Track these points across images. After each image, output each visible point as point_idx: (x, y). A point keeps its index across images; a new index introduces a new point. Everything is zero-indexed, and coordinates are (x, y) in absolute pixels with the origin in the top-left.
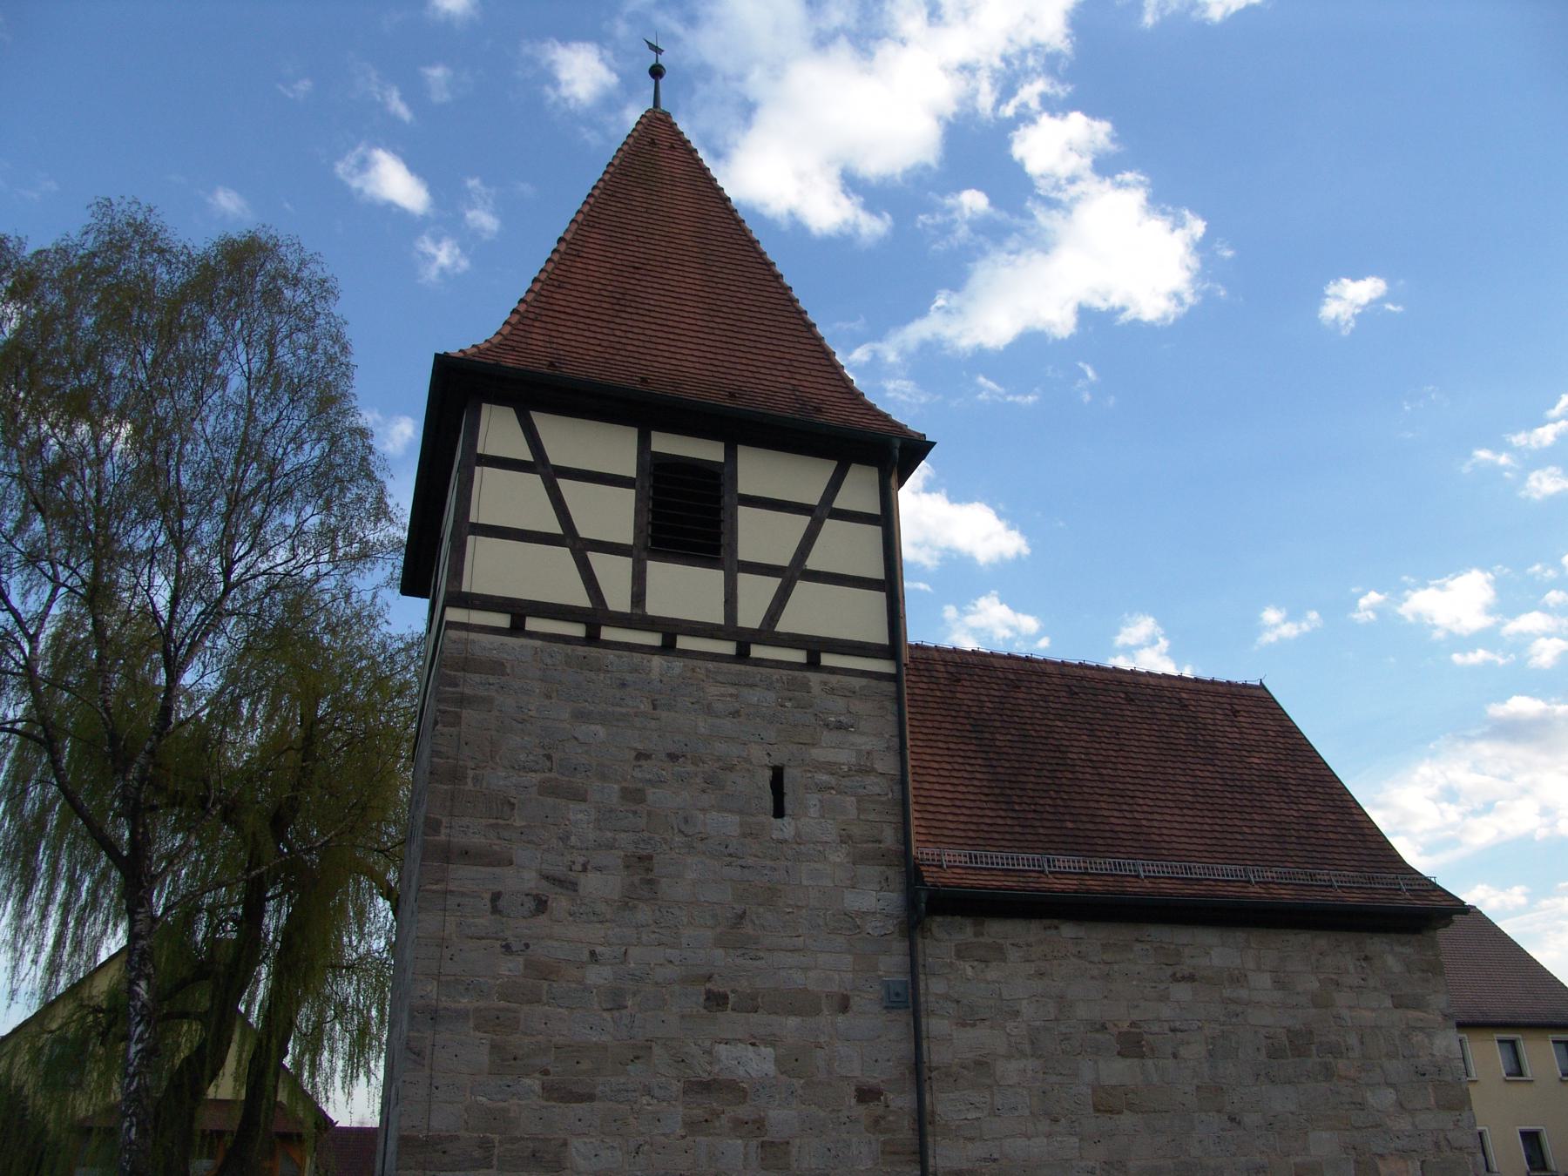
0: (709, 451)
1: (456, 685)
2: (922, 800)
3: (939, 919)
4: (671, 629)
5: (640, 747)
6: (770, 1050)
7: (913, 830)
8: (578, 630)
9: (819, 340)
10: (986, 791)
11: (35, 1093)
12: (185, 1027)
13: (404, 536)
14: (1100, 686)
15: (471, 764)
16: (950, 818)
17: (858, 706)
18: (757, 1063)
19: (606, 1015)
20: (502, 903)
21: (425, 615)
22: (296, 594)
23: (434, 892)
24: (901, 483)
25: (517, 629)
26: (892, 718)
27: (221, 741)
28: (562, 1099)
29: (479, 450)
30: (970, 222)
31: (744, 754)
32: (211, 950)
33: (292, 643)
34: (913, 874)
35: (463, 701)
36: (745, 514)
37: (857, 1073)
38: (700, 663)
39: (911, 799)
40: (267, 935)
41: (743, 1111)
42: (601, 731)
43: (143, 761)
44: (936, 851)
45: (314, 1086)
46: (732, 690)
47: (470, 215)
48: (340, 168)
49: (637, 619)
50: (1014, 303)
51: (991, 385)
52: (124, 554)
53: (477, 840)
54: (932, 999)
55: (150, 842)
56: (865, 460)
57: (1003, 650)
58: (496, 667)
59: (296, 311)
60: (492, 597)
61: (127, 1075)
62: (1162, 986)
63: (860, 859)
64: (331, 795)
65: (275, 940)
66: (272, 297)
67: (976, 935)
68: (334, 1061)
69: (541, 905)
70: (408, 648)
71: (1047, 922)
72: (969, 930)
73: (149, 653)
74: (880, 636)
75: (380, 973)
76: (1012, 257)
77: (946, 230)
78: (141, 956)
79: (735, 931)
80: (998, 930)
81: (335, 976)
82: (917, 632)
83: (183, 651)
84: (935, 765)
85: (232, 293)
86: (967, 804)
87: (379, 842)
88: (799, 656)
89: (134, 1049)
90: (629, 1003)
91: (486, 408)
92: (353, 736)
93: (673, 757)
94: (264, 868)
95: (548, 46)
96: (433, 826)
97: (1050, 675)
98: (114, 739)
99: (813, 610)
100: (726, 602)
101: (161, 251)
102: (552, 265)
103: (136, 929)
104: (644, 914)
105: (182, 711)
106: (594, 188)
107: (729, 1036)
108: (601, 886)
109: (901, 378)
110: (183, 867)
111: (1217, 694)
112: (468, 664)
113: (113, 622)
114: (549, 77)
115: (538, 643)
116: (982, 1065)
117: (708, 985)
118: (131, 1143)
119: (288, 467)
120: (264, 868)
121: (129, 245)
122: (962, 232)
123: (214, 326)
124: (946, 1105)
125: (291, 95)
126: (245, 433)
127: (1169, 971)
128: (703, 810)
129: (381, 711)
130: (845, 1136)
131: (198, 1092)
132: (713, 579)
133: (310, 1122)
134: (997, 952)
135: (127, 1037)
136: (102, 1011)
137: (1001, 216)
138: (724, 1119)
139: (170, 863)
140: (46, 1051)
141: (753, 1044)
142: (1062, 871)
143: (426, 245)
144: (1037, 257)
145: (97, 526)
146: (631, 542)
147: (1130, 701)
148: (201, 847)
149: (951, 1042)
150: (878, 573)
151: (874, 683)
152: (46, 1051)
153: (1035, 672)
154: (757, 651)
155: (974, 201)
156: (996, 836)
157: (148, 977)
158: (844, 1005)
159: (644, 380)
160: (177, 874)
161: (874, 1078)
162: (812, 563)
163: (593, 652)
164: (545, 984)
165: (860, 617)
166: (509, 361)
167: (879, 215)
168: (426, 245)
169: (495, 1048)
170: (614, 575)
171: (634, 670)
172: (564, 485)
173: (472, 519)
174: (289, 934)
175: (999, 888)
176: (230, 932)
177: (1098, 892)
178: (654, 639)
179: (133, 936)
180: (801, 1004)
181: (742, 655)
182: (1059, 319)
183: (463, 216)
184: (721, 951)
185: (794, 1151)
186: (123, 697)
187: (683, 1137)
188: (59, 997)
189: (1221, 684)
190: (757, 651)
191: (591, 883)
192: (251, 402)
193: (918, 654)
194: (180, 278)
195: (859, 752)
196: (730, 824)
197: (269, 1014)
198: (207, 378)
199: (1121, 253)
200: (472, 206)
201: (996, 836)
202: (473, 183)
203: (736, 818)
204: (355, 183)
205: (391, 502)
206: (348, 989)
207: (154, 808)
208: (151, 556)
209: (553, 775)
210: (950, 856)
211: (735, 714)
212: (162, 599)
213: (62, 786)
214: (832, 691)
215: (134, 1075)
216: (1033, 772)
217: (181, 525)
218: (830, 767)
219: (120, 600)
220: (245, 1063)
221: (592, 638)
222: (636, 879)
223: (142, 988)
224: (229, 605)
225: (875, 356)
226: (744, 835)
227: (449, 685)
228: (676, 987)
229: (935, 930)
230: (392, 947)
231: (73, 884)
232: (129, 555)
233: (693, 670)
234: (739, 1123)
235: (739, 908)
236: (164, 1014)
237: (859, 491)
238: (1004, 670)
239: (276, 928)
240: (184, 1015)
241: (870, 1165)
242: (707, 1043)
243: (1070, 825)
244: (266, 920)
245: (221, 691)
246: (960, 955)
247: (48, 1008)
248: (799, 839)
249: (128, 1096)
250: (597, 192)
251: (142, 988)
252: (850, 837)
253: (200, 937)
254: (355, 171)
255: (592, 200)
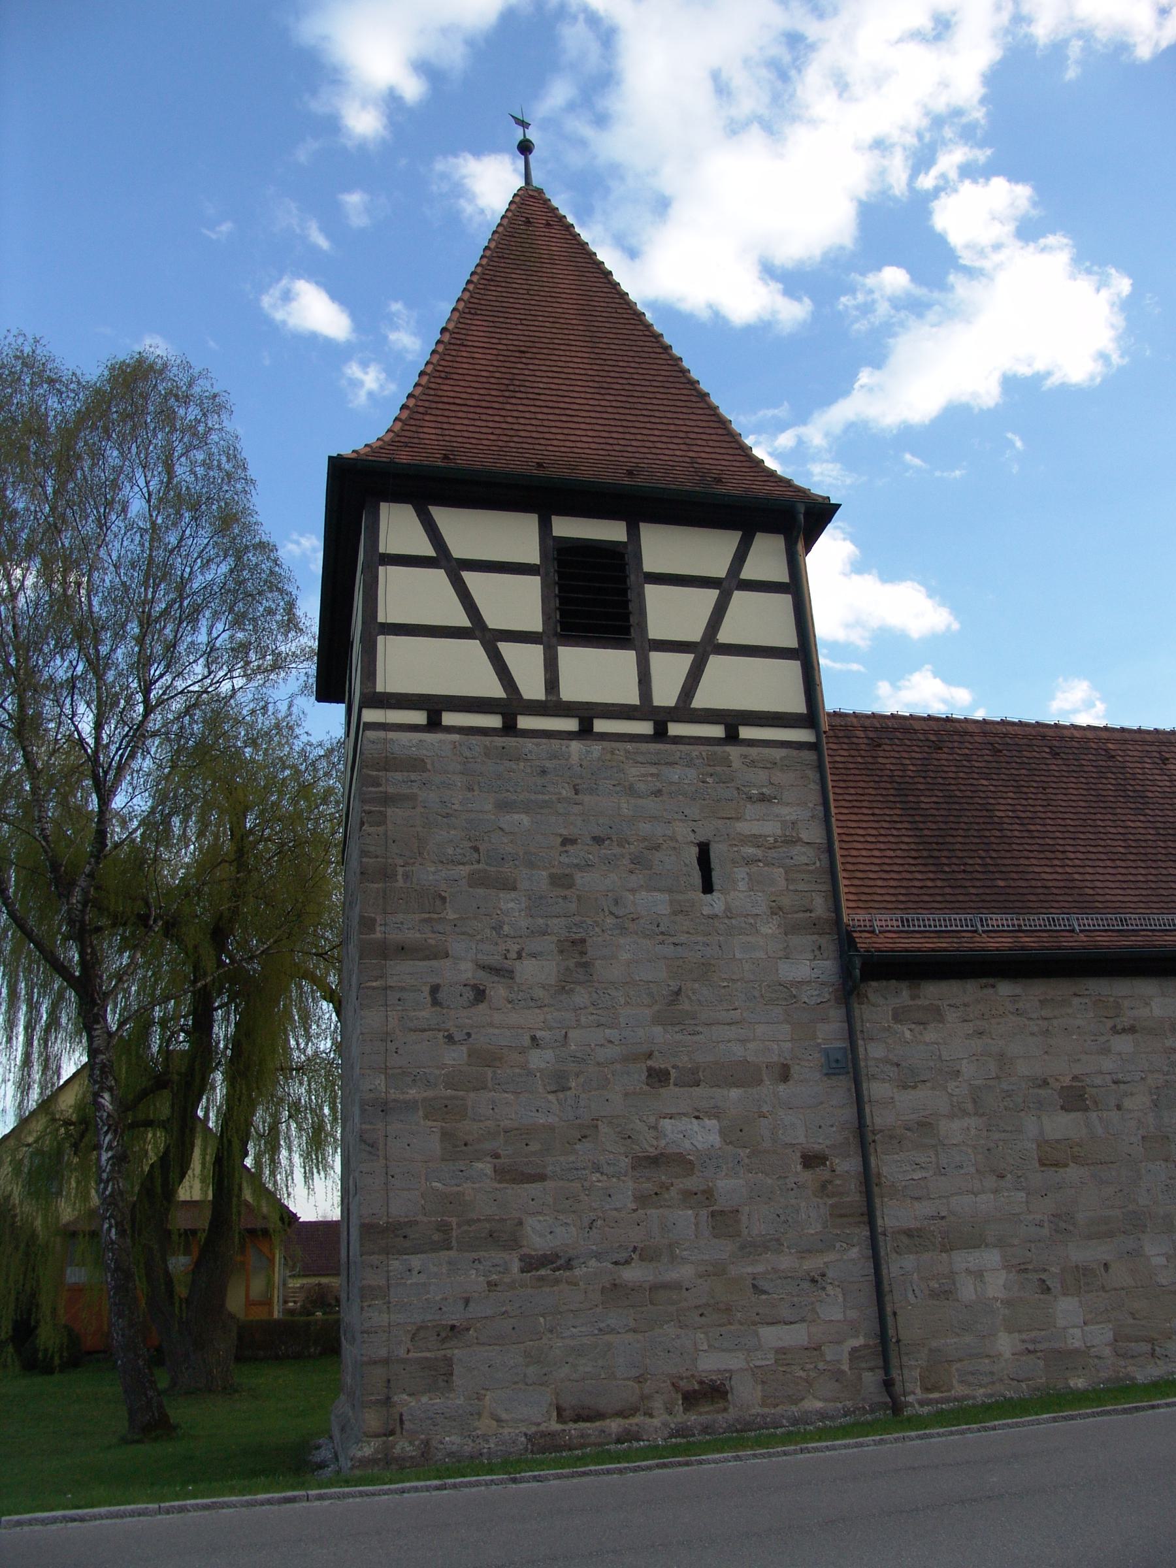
0: (612, 531)
1: (379, 785)
2: (850, 867)
3: (874, 984)
4: (586, 713)
5: (565, 832)
6: (714, 1122)
7: (843, 897)
8: (495, 721)
9: (713, 410)
10: (913, 854)
11: (21, 1203)
12: (150, 1135)
13: (315, 645)
14: (1025, 741)
15: (400, 862)
16: (880, 883)
17: (779, 777)
18: (703, 1136)
19: (551, 1097)
20: (441, 996)
21: (342, 719)
22: (216, 712)
23: (374, 988)
24: (808, 549)
25: (434, 724)
26: (815, 787)
27: (156, 859)
28: (514, 1181)
29: (382, 550)
30: (890, 300)
31: (669, 833)
32: (166, 1059)
33: (213, 759)
34: (846, 940)
35: (387, 800)
36: (652, 592)
37: (802, 1140)
38: (618, 745)
39: (839, 867)
40: (218, 1043)
41: (692, 1183)
42: (525, 819)
43: (84, 884)
44: (867, 917)
45: (275, 1182)
46: (653, 770)
47: (393, 336)
48: (266, 301)
49: (553, 706)
50: (933, 376)
51: (917, 462)
52: (46, 688)
53: (411, 935)
54: (871, 1063)
55: (99, 962)
56: (771, 528)
57: (922, 712)
58: (416, 764)
59: (192, 429)
60: (406, 695)
61: (101, 1181)
62: (1103, 1039)
63: (792, 929)
64: (267, 904)
65: (226, 1047)
66: (167, 417)
67: (913, 998)
68: (292, 1158)
69: (480, 995)
70: (330, 752)
71: (984, 981)
72: (905, 993)
73: (79, 781)
74: (797, 705)
75: (329, 1073)
76: (934, 330)
77: (867, 309)
78: (103, 1072)
79: (672, 1007)
80: (932, 991)
81: (286, 1079)
82: (834, 700)
83: (112, 773)
84: (861, 832)
85: (126, 417)
86: (896, 868)
87: (316, 946)
88: (717, 731)
89: (105, 1156)
90: (573, 1084)
91: (384, 507)
92: (283, 845)
93: (598, 840)
94: (209, 979)
95: (461, 161)
96: (368, 924)
97: (972, 734)
98: (55, 866)
99: (728, 685)
100: (640, 682)
101: (51, 381)
102: (437, 357)
103: (95, 1045)
104: (581, 997)
105: (117, 833)
106: (473, 274)
107: (674, 1111)
108: (537, 972)
109: (827, 461)
110: (134, 981)
111: (1144, 742)
112: (388, 763)
113: (41, 752)
114: (459, 190)
115: (456, 737)
116: (925, 1126)
117: (649, 1063)
118: (112, 1242)
119: (195, 586)
120: (209, 979)
121: (19, 379)
122: (883, 308)
123: (113, 455)
124: (891, 1166)
125: (214, 236)
126: (150, 555)
127: (1110, 1023)
128: (633, 891)
129: (309, 819)
130: (793, 1201)
131: (169, 1194)
132: (626, 659)
133: (275, 1217)
134: (936, 1014)
135: (97, 1147)
136: (72, 1124)
137: (920, 292)
138: (673, 1192)
139: (120, 980)
140: (26, 1161)
141: (697, 1118)
142: (995, 930)
143: (354, 370)
144: (864, 198)
145: (17, 661)
146: (541, 630)
147: (1056, 755)
148: (148, 963)
149: (892, 1105)
150: (792, 642)
151: (794, 753)
152: (26, 1161)
153: (957, 732)
154: (675, 729)
155: (894, 278)
156: (926, 898)
157: (110, 1089)
158: (784, 1074)
159: (540, 465)
160: (127, 991)
161: (819, 1143)
162: (723, 637)
163: (510, 741)
164: (489, 1072)
165: (769, 687)
166: (404, 457)
167: (799, 299)
168: (354, 370)
169: (446, 1135)
170: (527, 663)
171: (554, 756)
172: (471, 578)
173: (381, 619)
174: (236, 1043)
175: (933, 950)
176: (182, 1042)
177: (1033, 949)
178: (571, 725)
179: (92, 1052)
180: (742, 1075)
181: (660, 733)
182: (982, 388)
183: (386, 337)
184: (660, 1029)
185: (744, 1218)
186: (58, 825)
187: (635, 1211)
188: (32, 1113)
189: (1148, 732)
190: (675, 729)
191: (528, 970)
192: (154, 523)
193: (837, 721)
194: (72, 406)
195: (784, 823)
196: (660, 903)
197: (227, 1118)
198: (109, 504)
199: (1034, 314)
200: (396, 328)
201: (926, 898)
202: (396, 307)
203: (665, 897)
204: (279, 316)
205: (299, 613)
206: (299, 1090)
207: (99, 929)
208: (71, 684)
209: (480, 866)
210: (883, 920)
211: (658, 793)
212: (86, 726)
213: (11, 914)
214: (753, 764)
215: (108, 1181)
216: (961, 832)
217: (97, 651)
218: (756, 840)
219: (47, 730)
220: (209, 1165)
221: (509, 728)
222: (571, 963)
223: (106, 1099)
224: (151, 726)
225: (800, 441)
226: (675, 913)
227: (373, 786)
228: (618, 1066)
229: (871, 996)
230: (338, 1047)
231: (33, 1007)
232: (51, 686)
233: (613, 753)
234: (688, 1195)
235: (674, 984)
236: (130, 1120)
237: (767, 558)
238: (925, 732)
239: (226, 1035)
240: (149, 1124)
241: (819, 1228)
242: (652, 1120)
243: (1001, 883)
244: (216, 1029)
245: (153, 811)
246: (897, 1018)
247: (24, 1122)
248: (729, 913)
249: (104, 1200)
250: (475, 278)
251: (106, 1099)
252: (780, 909)
253: (155, 1049)
254: (279, 302)
255: (471, 287)
